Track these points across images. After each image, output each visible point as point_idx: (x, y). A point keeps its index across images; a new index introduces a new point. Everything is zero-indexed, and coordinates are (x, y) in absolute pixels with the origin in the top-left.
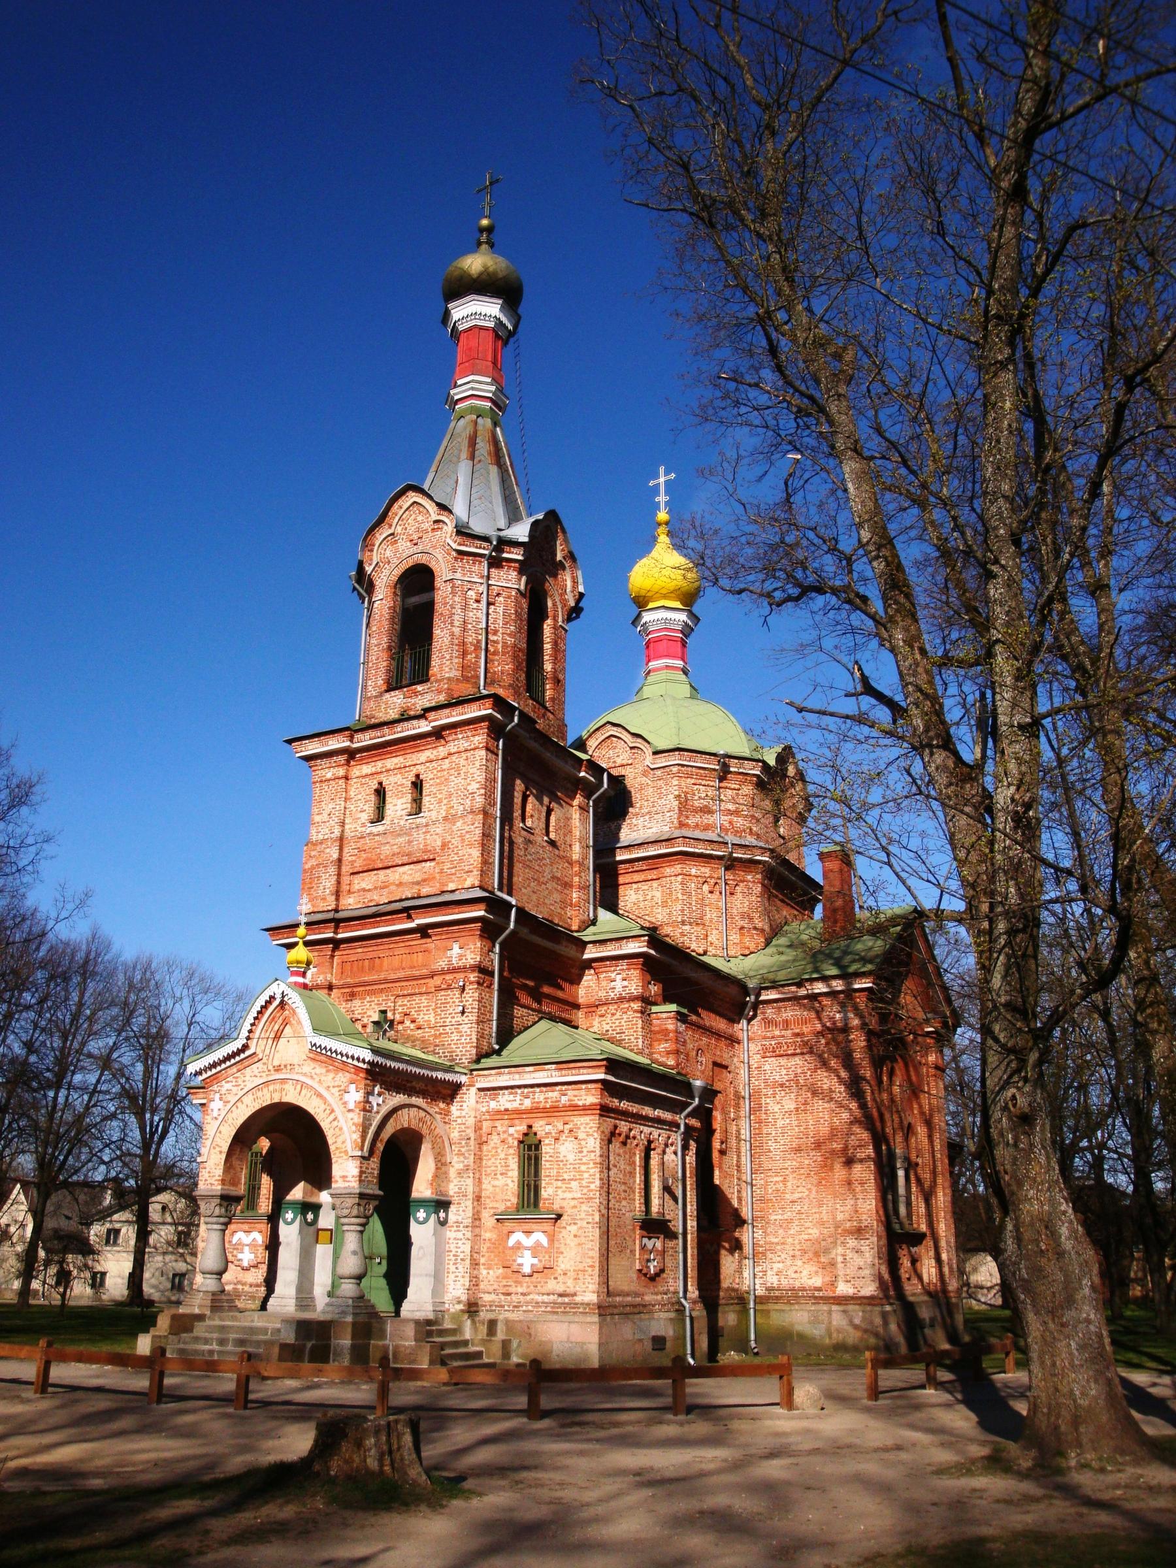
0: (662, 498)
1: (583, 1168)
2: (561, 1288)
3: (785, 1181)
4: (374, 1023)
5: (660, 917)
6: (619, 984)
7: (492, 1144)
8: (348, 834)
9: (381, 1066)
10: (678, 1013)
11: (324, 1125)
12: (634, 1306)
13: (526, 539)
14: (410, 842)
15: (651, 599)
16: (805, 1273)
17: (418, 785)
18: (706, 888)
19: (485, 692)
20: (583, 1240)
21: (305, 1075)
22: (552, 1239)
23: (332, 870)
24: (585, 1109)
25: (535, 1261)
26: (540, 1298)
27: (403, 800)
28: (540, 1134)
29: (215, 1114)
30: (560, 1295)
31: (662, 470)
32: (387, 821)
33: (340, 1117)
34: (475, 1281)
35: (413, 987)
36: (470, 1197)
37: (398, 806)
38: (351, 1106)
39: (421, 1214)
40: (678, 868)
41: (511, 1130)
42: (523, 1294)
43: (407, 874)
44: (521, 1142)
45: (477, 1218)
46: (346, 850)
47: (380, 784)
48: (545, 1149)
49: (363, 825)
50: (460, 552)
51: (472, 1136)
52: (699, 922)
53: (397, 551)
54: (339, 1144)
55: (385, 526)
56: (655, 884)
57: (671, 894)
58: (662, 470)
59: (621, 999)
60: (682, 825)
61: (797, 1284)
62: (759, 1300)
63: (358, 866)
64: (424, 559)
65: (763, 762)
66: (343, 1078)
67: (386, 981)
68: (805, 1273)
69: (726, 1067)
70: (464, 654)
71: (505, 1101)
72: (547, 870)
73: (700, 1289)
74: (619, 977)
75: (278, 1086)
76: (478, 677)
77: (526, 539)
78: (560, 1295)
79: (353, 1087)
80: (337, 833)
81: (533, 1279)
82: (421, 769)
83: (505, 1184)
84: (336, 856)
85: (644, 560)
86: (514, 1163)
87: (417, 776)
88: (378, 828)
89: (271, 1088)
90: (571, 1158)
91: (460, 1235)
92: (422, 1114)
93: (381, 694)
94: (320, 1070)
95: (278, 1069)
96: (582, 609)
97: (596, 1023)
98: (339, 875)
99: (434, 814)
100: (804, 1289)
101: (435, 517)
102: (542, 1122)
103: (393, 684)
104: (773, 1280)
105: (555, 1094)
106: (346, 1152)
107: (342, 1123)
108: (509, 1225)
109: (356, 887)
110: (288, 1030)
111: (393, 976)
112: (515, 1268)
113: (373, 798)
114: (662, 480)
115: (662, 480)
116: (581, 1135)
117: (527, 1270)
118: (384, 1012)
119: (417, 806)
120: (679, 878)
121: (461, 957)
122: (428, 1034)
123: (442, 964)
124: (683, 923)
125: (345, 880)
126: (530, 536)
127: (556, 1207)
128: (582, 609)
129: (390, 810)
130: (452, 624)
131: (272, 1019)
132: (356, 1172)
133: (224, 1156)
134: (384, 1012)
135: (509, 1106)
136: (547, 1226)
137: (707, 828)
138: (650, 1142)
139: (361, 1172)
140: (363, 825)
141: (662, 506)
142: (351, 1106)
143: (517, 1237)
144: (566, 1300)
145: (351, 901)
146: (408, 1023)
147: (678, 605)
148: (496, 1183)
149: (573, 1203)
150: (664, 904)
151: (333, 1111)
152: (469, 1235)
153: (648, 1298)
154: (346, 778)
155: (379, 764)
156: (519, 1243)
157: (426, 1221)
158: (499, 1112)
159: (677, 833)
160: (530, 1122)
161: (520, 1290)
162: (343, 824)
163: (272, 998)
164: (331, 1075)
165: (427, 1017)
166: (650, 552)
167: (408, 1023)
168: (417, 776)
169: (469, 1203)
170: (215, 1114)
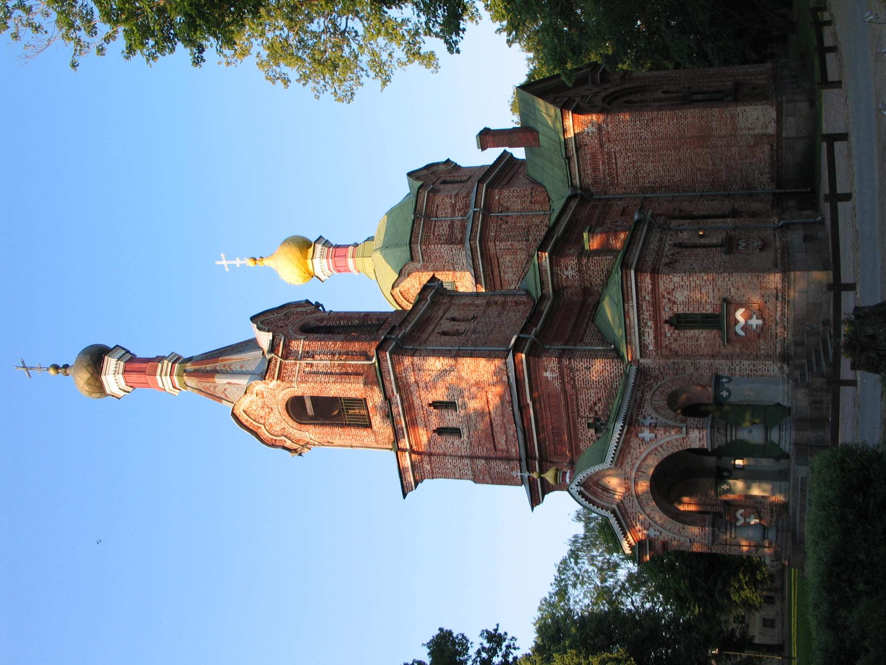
0: (238, 262)
1: (693, 284)
3: (700, 170)
4: (596, 432)
5: (523, 257)
6: (570, 273)
7: (677, 348)
8: (468, 453)
9: (625, 418)
10: (589, 232)
11: (665, 454)
13: (271, 334)
16: (761, 156)
19: (374, 360)
20: (740, 284)
22: (740, 305)
23: (493, 463)
24: (655, 283)
26: (779, 314)
27: (446, 415)
28: (670, 314)
29: (658, 533)
30: (777, 299)
31: (218, 263)
32: (459, 426)
33: (660, 443)
34: (768, 357)
35: (572, 405)
36: (712, 361)
38: (653, 435)
39: (724, 394)
40: (491, 244)
41: (668, 335)
42: (776, 325)
44: (676, 328)
45: (726, 357)
46: (479, 454)
49: (463, 442)
50: (278, 378)
51: (672, 361)
52: (527, 230)
53: (276, 423)
54: (678, 444)
55: (259, 431)
56: (501, 260)
57: (508, 249)
58: (218, 263)
59: (579, 271)
60: (462, 242)
61: (769, 161)
63: (490, 446)
64: (281, 407)
65: (419, 188)
66: (634, 443)
67: (568, 424)
68: (761, 156)
69: (624, 208)
70: (347, 374)
71: (649, 339)
74: (565, 273)
77: (271, 334)
79: (640, 435)
81: (766, 317)
83: (703, 337)
84: (483, 462)
85: (280, 273)
86: (690, 333)
87: (430, 405)
88: (465, 432)
90: (686, 293)
91: (738, 368)
92: (658, 393)
93: (374, 432)
94: (629, 459)
96: (317, 303)
97: (596, 289)
98: (496, 459)
100: (772, 156)
102: (663, 314)
103: (369, 426)
104: (766, 178)
105: (644, 304)
106: (684, 438)
107: (663, 441)
108: (731, 336)
109: (504, 447)
111: (565, 420)
112: (759, 330)
113: (444, 437)
114: (225, 263)
115: (225, 263)
117: (760, 322)
121: (552, 371)
122: (603, 394)
123: (557, 384)
124: (527, 240)
125: (499, 454)
126: (268, 331)
127: (718, 302)
128: (317, 303)
131: (594, 493)
132: (696, 432)
135: (652, 336)
136: (732, 307)
137: (463, 226)
138: (675, 245)
139: (697, 427)
140: (463, 442)
141: (242, 262)
142: (653, 435)
144: (780, 294)
145: (513, 450)
146: (597, 408)
147: (311, 249)
148: (703, 345)
149: (716, 291)
150: (515, 253)
151: (656, 449)
152: (738, 362)
153: (778, 244)
156: (742, 329)
157: (728, 390)
158: (656, 343)
159: (467, 245)
160: (662, 322)
161: (773, 327)
162: (462, 457)
163: (580, 493)
164: (632, 451)
165: (592, 395)
166: (274, 270)
167: (597, 408)
169: (716, 362)
170: (658, 533)
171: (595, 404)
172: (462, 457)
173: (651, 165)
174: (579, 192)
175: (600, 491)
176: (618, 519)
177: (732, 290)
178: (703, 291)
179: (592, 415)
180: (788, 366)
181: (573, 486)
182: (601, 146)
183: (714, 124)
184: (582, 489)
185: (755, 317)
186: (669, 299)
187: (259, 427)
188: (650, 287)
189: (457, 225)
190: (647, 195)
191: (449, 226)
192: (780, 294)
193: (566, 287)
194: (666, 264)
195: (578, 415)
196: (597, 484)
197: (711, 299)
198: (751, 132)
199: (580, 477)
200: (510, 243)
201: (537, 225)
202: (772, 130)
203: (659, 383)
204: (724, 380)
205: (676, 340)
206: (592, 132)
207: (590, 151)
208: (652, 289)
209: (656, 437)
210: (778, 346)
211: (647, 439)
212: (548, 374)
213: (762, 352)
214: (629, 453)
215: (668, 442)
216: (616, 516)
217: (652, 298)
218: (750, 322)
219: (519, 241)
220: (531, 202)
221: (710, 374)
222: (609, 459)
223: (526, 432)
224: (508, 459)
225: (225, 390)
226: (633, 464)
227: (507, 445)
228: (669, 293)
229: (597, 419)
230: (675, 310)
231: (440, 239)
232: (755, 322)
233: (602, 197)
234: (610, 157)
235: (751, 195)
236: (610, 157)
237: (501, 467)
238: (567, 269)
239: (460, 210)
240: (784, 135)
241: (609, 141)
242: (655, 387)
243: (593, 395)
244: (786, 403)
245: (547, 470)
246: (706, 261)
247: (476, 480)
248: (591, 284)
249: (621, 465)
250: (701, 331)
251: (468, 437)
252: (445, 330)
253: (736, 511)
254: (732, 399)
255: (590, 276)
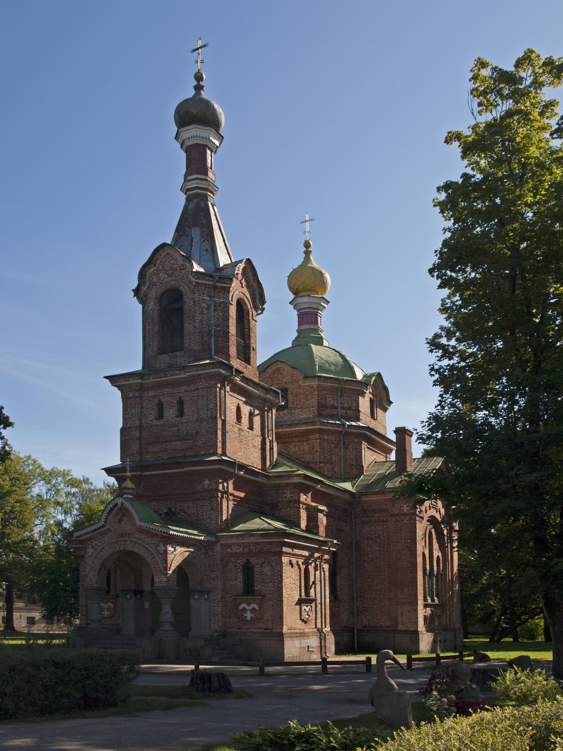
1: (275, 578)
2: (266, 627)
4: (165, 513)
5: (308, 459)
12: (300, 633)
14: (178, 430)
15: (300, 292)
17: (181, 403)
18: (332, 445)
21: (136, 538)
25: (253, 615)
26: (254, 630)
27: (173, 410)
30: (265, 629)
37: (170, 413)
40: (317, 436)
41: (239, 561)
43: (178, 445)
47: (160, 401)
48: (257, 569)
49: (152, 421)
56: (305, 443)
57: (313, 448)
59: (290, 501)
60: (320, 415)
62: (359, 631)
69: (343, 530)
70: (203, 337)
71: (235, 550)
72: (250, 442)
73: (330, 627)
74: (288, 492)
75: (122, 543)
76: (211, 349)
78: (265, 629)
80: (137, 423)
82: (182, 395)
83: (239, 583)
86: (240, 576)
88: (160, 422)
89: (119, 543)
90: (269, 573)
95: (121, 536)
96: (264, 309)
99: (191, 417)
101: (180, 262)
106: (160, 572)
107: (158, 558)
110: (125, 518)
116: (273, 564)
117: (249, 618)
118: (170, 509)
119: (181, 413)
120: (318, 441)
121: (209, 485)
123: (200, 488)
128: (264, 309)
129: (166, 414)
130: (194, 321)
131: (117, 514)
133: (97, 572)
134: (170, 509)
135: (237, 551)
138: (208, 592)
140: (152, 421)
143: (244, 605)
144: (268, 631)
145: (148, 457)
148: (232, 583)
149: (270, 592)
150: (310, 453)
151: (152, 554)
153: (307, 630)
154: (141, 397)
155: (159, 391)
157: (198, 599)
162: (140, 420)
163: (116, 505)
164: (150, 539)
168: (180, 398)
169: (219, 592)
170: (90, 554)
171: (186, 513)
172: (140, 420)
173: (377, 548)
174: (357, 500)
175: (119, 517)
176: (98, 529)
177: (271, 602)
178: (270, 584)
179: (177, 511)
180: (218, 635)
181: (121, 500)
182: (392, 516)
183: (406, 591)
184: (119, 506)
185: (253, 615)
186: (264, 562)
187: (155, 266)
188: (273, 551)
189: (334, 411)
190: (354, 546)
191: (333, 405)
192: (268, 631)
193: (278, 493)
194: (290, 561)
195: (177, 501)
196: (124, 515)
197: (265, 589)
198: (399, 615)
199: (128, 505)
200: (319, 450)
201: (333, 469)
202: (400, 627)
203: (202, 555)
204: (206, 596)
205: (235, 566)
206: (403, 510)
207: (389, 508)
208: (271, 552)
209: (161, 554)
210: (233, 630)
211: (159, 548)
212: (207, 482)
213: (228, 620)
214: (148, 537)
215: (157, 562)
216: (101, 528)
217: (265, 551)
218: (249, 612)
219: (320, 456)
220: (352, 465)
221: (210, 587)
222: (143, 524)
223: (163, 466)
224: (141, 453)
225: (187, 236)
226: (140, 540)
227: (152, 452)
228: (268, 562)
229: (174, 514)
230: (257, 566)
231: (322, 399)
232: (249, 615)
233: (353, 515)
234: (384, 521)
235: (353, 613)
236: (384, 521)
237: (134, 448)
238: (291, 493)
239: (346, 413)
240: (396, 635)
241: (396, 521)
242: (199, 553)
243: (193, 512)
244: (190, 634)
245: (132, 482)
246: (293, 586)
247: (123, 431)
248: (280, 509)
249: (139, 532)
250: (242, 582)
251: (156, 425)
252: (242, 409)
253: (112, 603)
254: (192, 602)
255: (286, 509)
